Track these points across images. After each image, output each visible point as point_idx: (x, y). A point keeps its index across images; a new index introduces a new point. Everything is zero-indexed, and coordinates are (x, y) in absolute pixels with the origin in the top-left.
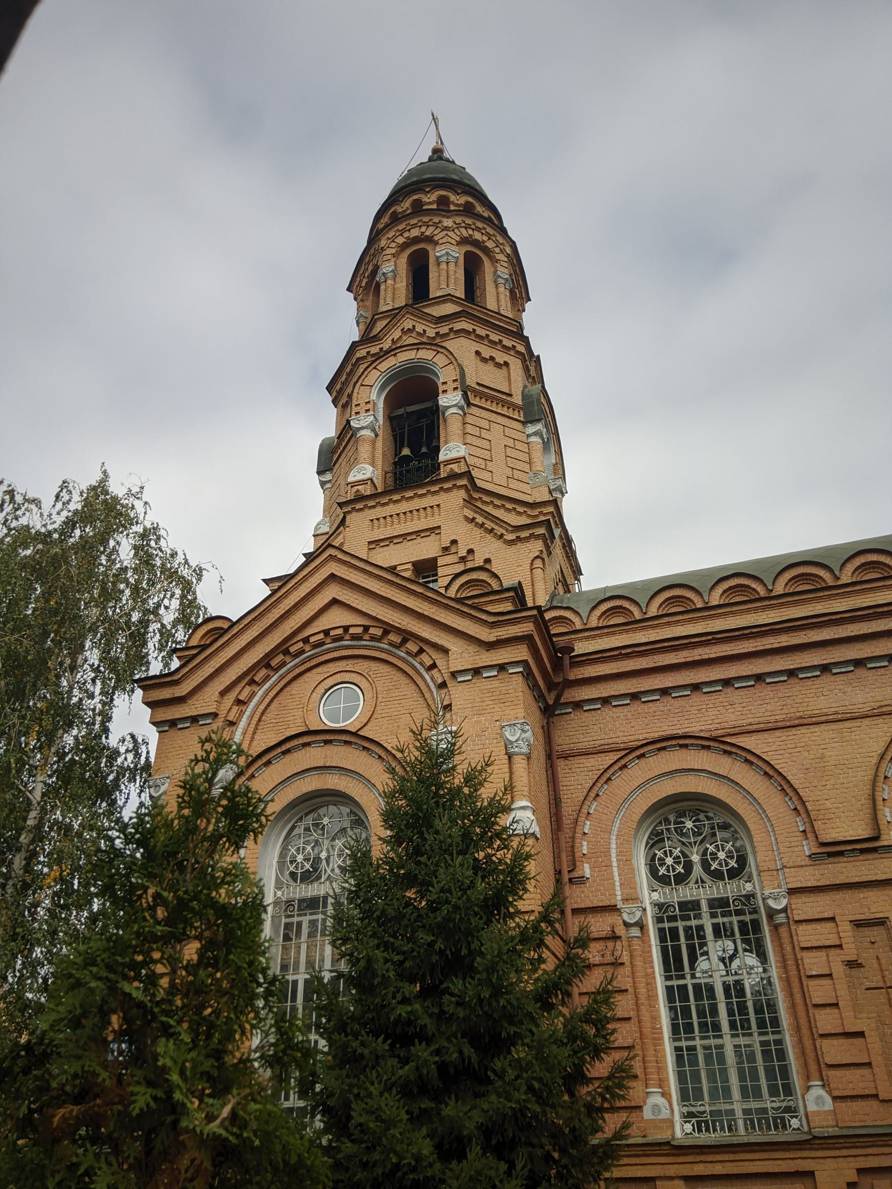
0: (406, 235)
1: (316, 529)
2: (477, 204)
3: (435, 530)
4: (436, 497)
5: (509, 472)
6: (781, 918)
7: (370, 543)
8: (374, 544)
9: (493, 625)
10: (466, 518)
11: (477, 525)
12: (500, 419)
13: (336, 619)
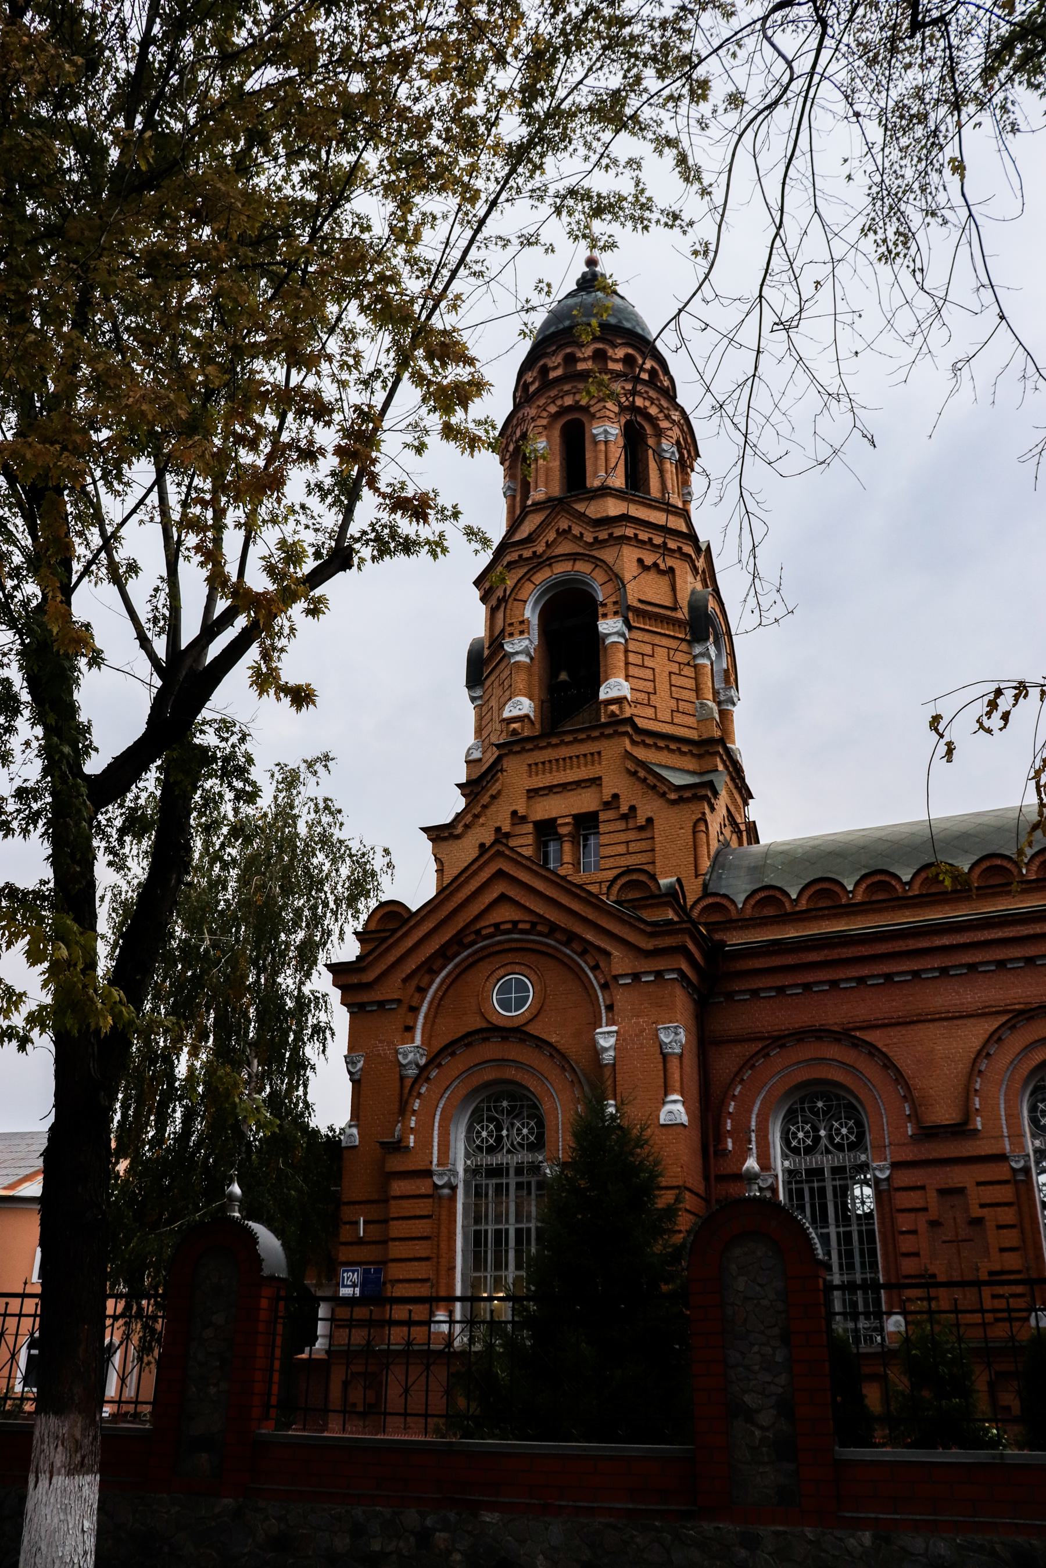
0: (559, 402)
1: (468, 754)
2: (638, 356)
3: (596, 782)
4: (597, 743)
5: (673, 704)
6: (884, 1186)
7: (528, 791)
8: (533, 793)
9: (652, 935)
10: (628, 771)
11: (639, 778)
12: (665, 642)
13: (505, 914)
